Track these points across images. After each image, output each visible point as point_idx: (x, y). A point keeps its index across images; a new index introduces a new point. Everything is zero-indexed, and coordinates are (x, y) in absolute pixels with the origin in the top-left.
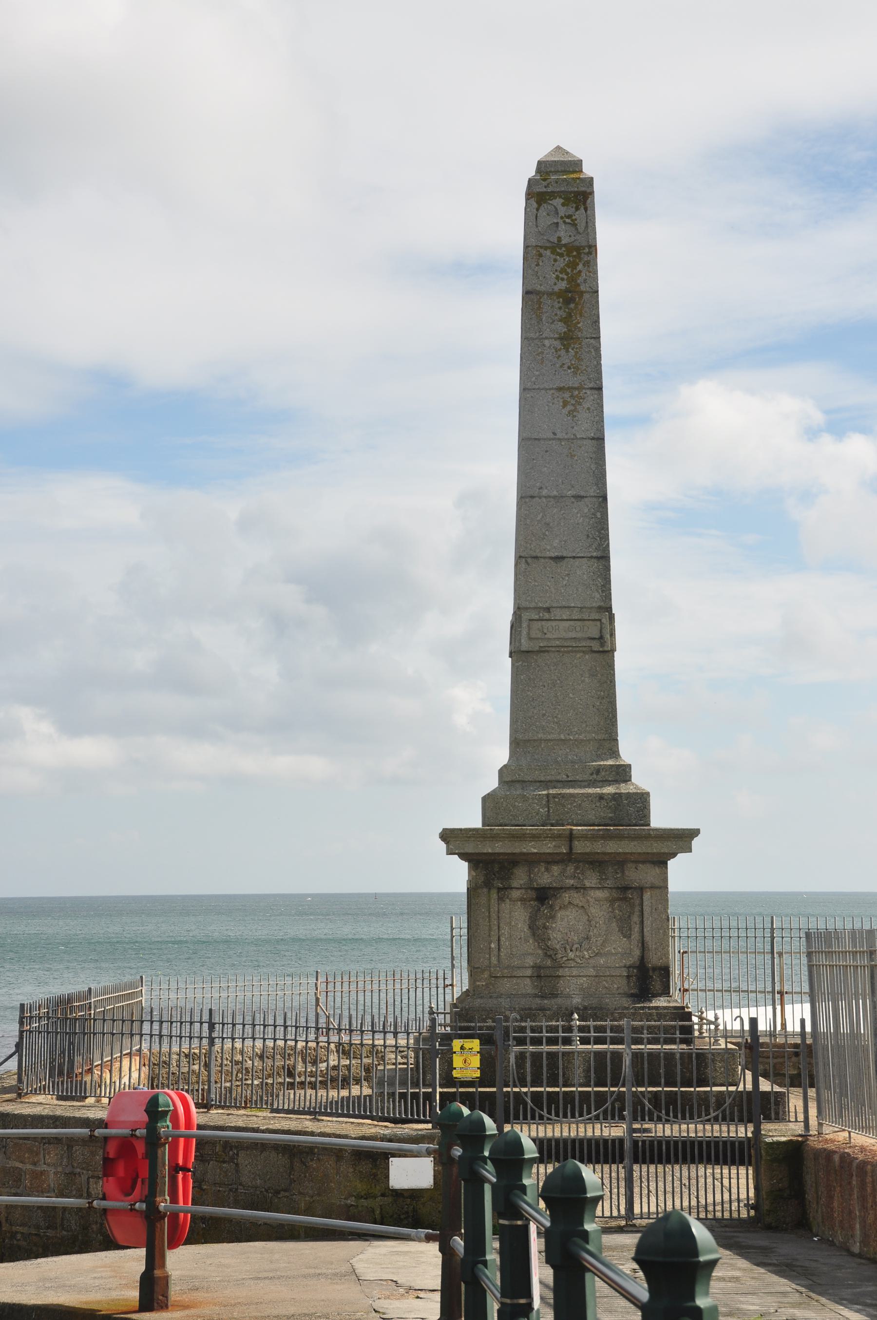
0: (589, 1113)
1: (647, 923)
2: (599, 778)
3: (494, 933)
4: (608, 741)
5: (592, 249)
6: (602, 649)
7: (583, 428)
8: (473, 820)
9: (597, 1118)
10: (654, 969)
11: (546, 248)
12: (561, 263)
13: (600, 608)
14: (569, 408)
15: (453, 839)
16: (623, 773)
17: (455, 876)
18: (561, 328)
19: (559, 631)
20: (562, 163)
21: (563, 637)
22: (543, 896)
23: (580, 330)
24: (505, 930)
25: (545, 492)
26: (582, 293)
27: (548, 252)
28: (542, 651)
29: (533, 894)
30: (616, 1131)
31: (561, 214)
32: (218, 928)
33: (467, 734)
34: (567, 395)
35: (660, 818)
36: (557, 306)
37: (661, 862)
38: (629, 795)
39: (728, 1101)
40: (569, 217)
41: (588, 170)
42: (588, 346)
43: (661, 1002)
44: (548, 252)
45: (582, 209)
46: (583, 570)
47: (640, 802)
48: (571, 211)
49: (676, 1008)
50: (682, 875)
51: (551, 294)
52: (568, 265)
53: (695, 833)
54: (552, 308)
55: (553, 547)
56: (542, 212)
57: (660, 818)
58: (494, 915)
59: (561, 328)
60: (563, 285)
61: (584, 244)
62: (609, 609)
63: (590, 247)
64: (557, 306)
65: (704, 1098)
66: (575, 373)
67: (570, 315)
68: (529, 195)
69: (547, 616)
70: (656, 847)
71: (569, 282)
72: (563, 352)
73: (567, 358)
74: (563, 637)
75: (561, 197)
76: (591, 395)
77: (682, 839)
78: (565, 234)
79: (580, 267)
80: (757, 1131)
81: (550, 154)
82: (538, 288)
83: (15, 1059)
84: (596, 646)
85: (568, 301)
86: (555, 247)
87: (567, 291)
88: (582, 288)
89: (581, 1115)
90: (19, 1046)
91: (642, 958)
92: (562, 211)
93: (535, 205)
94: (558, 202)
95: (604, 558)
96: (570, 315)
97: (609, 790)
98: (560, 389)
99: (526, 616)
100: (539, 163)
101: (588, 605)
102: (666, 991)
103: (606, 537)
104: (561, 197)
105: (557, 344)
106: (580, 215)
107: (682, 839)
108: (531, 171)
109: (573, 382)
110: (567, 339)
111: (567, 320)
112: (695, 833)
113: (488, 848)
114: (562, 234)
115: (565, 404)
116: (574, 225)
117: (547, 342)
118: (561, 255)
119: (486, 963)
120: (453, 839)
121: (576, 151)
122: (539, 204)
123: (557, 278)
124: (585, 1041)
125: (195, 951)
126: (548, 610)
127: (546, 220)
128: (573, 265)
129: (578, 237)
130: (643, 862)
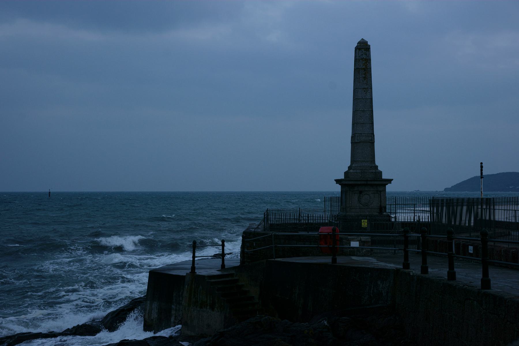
4: (374, 161)
5: (370, 60)
6: (372, 142)
8: (342, 177)
12: (364, 62)
15: (338, 181)
17: (338, 188)
18: (364, 76)
22: (361, 192)
32: (178, 266)
33: (341, 161)
35: (384, 177)
37: (385, 185)
47: (381, 173)
50: (389, 188)
53: (392, 180)
57: (384, 177)
59: (364, 76)
60: (364, 67)
62: (373, 134)
70: (384, 183)
75: (363, 50)
77: (389, 181)
78: (364, 56)
80: (334, 260)
85: (365, 70)
86: (362, 59)
94: (363, 50)
95: (373, 123)
97: (374, 171)
102: (385, 211)
103: (373, 119)
104: (363, 50)
106: (367, 53)
107: (389, 181)
110: (365, 78)
112: (392, 180)
120: (338, 181)
121: (366, 39)
125: (174, 269)
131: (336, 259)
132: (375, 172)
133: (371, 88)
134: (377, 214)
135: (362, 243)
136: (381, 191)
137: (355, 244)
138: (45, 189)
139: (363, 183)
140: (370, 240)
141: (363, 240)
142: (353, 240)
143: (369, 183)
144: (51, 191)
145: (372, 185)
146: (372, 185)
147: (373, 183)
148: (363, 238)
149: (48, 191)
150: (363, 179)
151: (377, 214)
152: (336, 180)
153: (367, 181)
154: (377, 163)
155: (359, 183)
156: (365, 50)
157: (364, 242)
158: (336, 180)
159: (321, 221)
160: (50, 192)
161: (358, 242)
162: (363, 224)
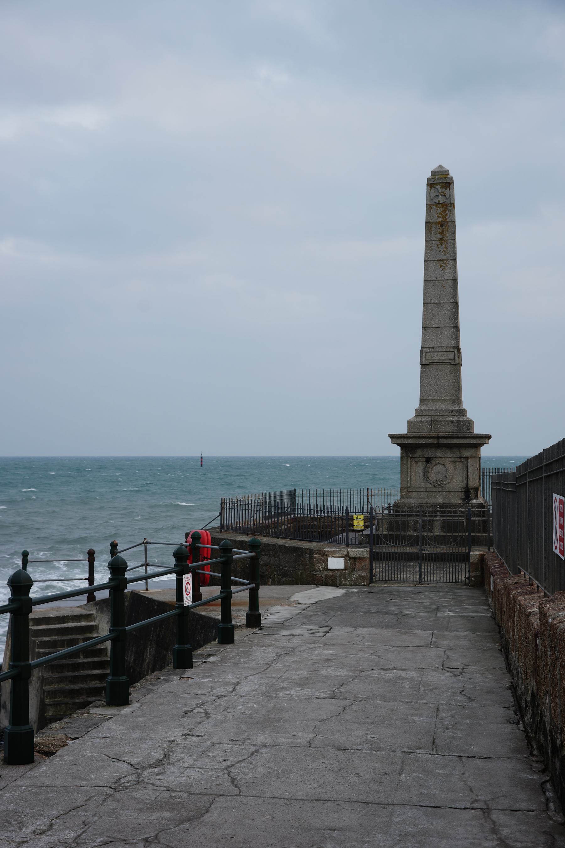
0: (402, 544)
1: (470, 470)
2: (452, 414)
3: (409, 474)
4: (458, 399)
5: (453, 205)
7: (448, 275)
9: (408, 544)
10: (472, 489)
11: (434, 205)
12: (440, 210)
13: (454, 347)
14: (442, 268)
15: (394, 438)
16: (462, 412)
17: (396, 451)
18: (439, 236)
19: (437, 357)
20: (440, 171)
21: (441, 360)
22: (428, 460)
23: (447, 237)
24: (413, 473)
25: (432, 301)
26: (448, 222)
27: (434, 207)
28: (431, 364)
29: (424, 459)
30: (413, 550)
31: (440, 191)
33: (400, 403)
34: (442, 263)
36: (438, 227)
38: (463, 421)
39: (413, 538)
40: (443, 192)
41: (451, 174)
42: (450, 243)
43: (474, 501)
44: (434, 207)
45: (448, 189)
46: (448, 332)
47: (469, 424)
48: (444, 190)
49: (479, 504)
50: (485, 451)
51: (435, 223)
52: (442, 212)
54: (436, 229)
55: (435, 323)
56: (432, 191)
57: (478, 430)
58: (409, 467)
59: (439, 236)
60: (440, 219)
61: (449, 203)
63: (451, 204)
64: (438, 227)
65: (404, 537)
66: (445, 254)
67: (443, 231)
68: (428, 185)
69: (433, 350)
71: (443, 218)
72: (440, 246)
73: (442, 248)
74: (441, 360)
75: (440, 185)
76: (451, 263)
78: (441, 199)
79: (447, 212)
81: (436, 168)
82: (430, 221)
83: (219, 518)
84: (452, 362)
85: (442, 226)
86: (437, 204)
87: (442, 221)
88: (448, 220)
89: (402, 544)
90: (221, 514)
91: (467, 484)
92: (440, 190)
93: (429, 188)
94: (438, 187)
96: (443, 231)
97: (456, 419)
98: (440, 260)
99: (424, 350)
100: (432, 172)
101: (449, 346)
102: (476, 497)
104: (440, 185)
105: (438, 243)
106: (447, 192)
108: (429, 175)
109: (444, 257)
111: (442, 233)
112: (489, 437)
113: (406, 442)
114: (440, 199)
115: (441, 266)
116: (445, 195)
117: (434, 242)
118: (440, 208)
119: (406, 486)
120: (394, 438)
121: (446, 166)
122: (431, 188)
123: (438, 216)
124: (441, 516)
126: (433, 348)
127: (433, 195)
128: (444, 211)
129: (447, 200)
130: (468, 447)
131: (230, 594)
132: (458, 422)
133: (455, 260)
134: (460, 501)
135: (351, 560)
136: (467, 458)
137: (336, 563)
138: (194, 452)
139: (430, 441)
140: (367, 555)
141: (352, 554)
142: (333, 554)
143: (442, 441)
144: (203, 455)
145: (450, 447)
146: (450, 447)
147: (449, 441)
148: (354, 552)
149: (200, 456)
150: (439, 436)
151: (460, 501)
152: (391, 436)
153: (438, 438)
154: (465, 406)
155: (423, 442)
156: (442, 187)
157: (355, 558)
158: (391, 436)
159: (302, 515)
160: (202, 458)
161: (342, 560)
162: (355, 523)
